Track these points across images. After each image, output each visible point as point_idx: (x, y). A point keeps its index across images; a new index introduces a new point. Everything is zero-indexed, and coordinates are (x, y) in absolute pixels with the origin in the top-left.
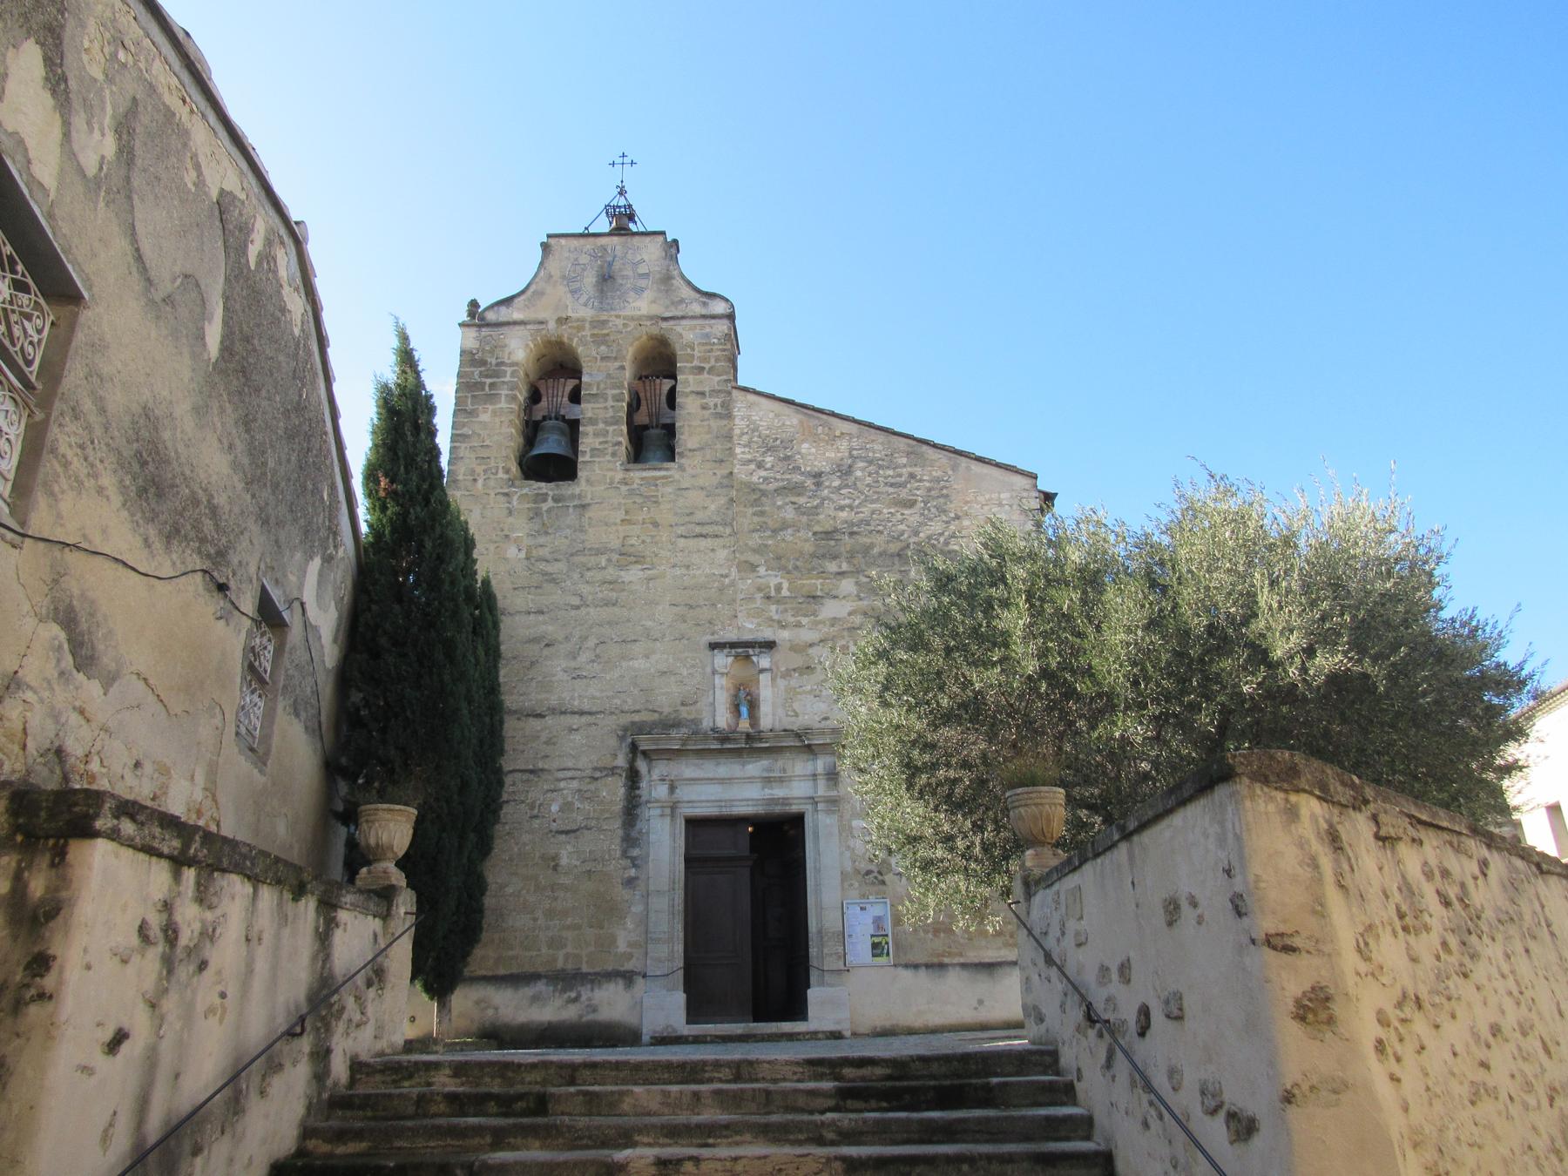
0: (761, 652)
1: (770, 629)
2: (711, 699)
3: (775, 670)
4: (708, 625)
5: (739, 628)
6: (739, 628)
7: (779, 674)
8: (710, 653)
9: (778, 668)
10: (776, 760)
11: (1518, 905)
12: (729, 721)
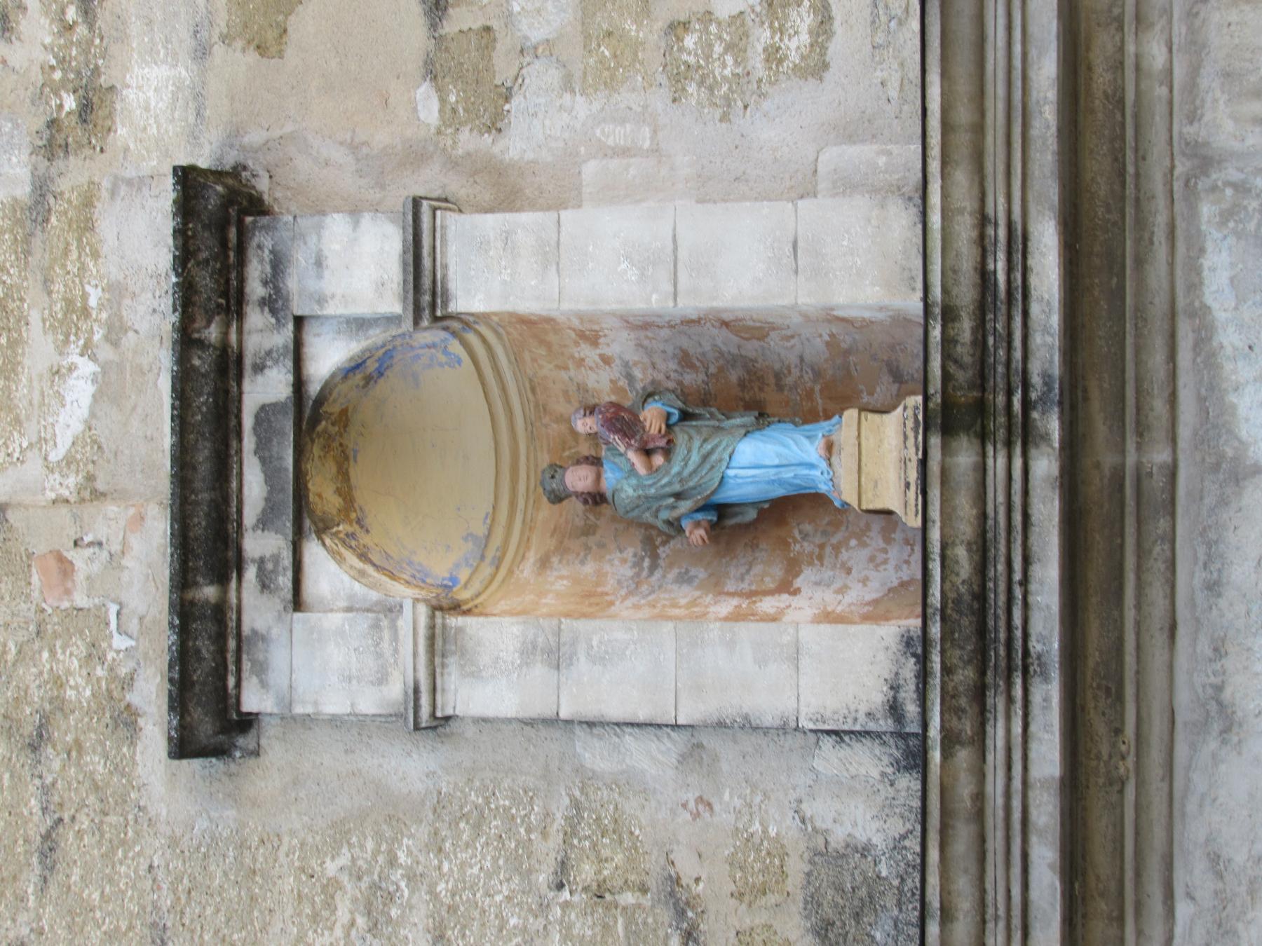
0: (274, 303)
1: (107, 225)
2: (664, 751)
3: (427, 181)
4: (53, 760)
5: (92, 493)
6: (92, 493)
7: (468, 141)
8: (270, 736)
9: (415, 156)
10: (1205, 160)
11: (207, 8)
12: (858, 594)
